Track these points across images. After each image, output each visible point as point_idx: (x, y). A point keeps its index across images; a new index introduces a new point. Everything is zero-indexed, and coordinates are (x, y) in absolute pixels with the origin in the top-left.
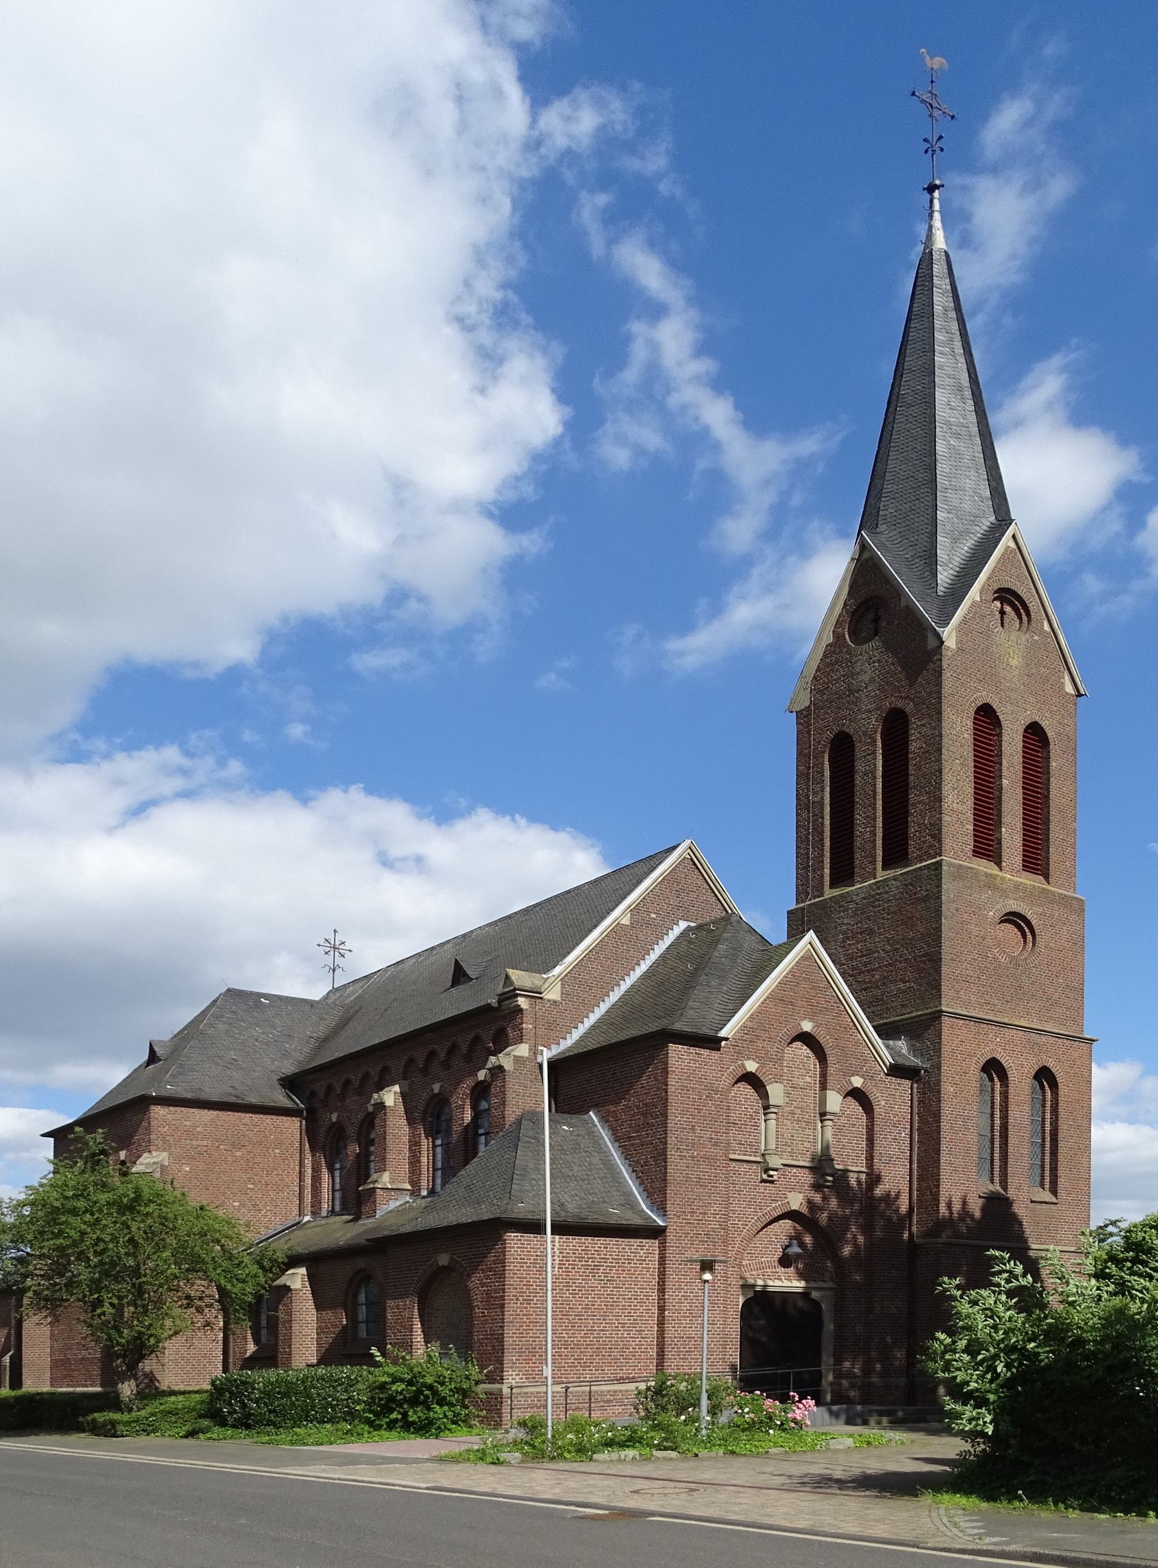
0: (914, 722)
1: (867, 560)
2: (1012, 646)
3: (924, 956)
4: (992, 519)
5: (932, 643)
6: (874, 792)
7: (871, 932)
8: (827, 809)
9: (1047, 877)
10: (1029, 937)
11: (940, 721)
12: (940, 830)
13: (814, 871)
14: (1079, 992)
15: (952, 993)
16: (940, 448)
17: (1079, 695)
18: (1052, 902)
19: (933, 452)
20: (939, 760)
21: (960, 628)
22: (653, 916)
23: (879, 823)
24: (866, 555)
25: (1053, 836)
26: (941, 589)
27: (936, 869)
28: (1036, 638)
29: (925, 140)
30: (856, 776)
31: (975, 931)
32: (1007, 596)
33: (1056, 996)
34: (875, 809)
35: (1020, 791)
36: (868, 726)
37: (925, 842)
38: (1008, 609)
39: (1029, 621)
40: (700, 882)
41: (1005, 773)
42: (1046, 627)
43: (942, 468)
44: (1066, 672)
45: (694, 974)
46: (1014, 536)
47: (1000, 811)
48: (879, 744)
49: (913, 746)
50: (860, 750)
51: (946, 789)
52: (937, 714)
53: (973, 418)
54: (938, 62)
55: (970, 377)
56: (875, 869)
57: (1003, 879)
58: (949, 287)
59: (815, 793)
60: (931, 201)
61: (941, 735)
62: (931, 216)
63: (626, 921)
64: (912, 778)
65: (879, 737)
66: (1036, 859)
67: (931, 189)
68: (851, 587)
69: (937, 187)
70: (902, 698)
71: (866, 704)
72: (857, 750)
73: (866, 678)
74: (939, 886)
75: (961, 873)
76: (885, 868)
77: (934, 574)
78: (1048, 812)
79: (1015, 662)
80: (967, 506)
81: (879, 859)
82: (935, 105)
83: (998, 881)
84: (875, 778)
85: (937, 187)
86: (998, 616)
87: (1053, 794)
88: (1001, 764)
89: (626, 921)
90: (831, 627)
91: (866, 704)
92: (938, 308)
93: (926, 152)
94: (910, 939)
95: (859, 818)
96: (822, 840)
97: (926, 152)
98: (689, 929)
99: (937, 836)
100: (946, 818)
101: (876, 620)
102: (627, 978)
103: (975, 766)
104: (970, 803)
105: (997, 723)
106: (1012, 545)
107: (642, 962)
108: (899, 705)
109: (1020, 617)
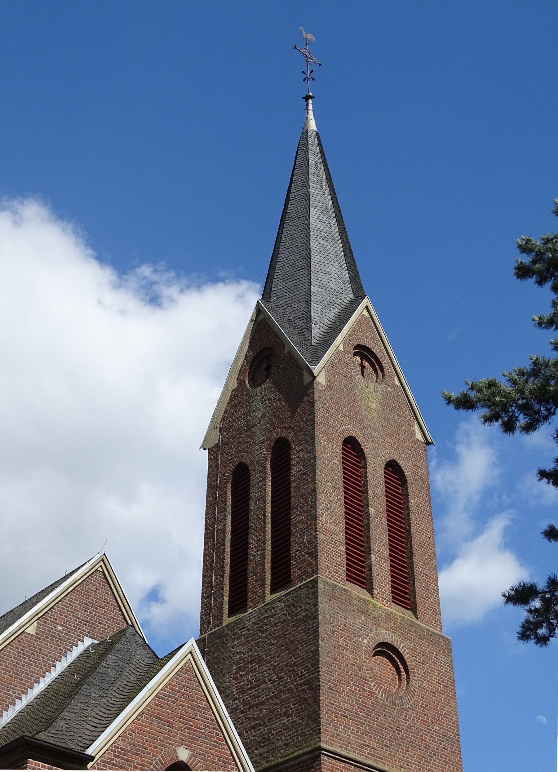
0: (295, 448)
1: (261, 321)
2: (370, 393)
3: (304, 684)
4: (352, 296)
5: (307, 379)
6: (264, 515)
7: (260, 660)
8: (228, 537)
9: (414, 611)
10: (403, 673)
11: (314, 444)
12: (316, 547)
13: (215, 599)
14: (454, 742)
15: (331, 729)
17: (428, 443)
18: (421, 637)
20: (314, 480)
21: (331, 365)
22: (60, 628)
23: (268, 546)
24: (261, 317)
25: (417, 570)
27: (313, 587)
28: (389, 389)
29: (303, 72)
30: (251, 502)
31: (351, 658)
32: (363, 352)
33: (434, 746)
34: (264, 532)
36: (261, 455)
37: (304, 561)
38: (366, 364)
39: (383, 375)
40: (109, 598)
41: (371, 502)
42: (397, 382)
43: (315, 258)
44: (415, 422)
45: (79, 684)
47: (368, 537)
49: (294, 470)
50: (255, 477)
51: (320, 508)
52: (310, 439)
53: (336, 229)
54: (309, 36)
55: (333, 203)
56: (264, 593)
57: (375, 606)
58: (319, 151)
59: (219, 521)
60: (307, 105)
61: (314, 458)
62: (307, 112)
63: (31, 630)
64: (293, 499)
65: (268, 465)
66: (404, 592)
67: (307, 98)
70: (286, 428)
71: (260, 436)
72: (252, 478)
73: (259, 414)
74: (316, 605)
75: (335, 594)
76: (273, 591)
77: (309, 330)
78: (411, 546)
79: (374, 406)
80: (333, 285)
81: (268, 582)
82: (309, 56)
83: (370, 607)
84: (265, 502)
86: (359, 368)
87: (414, 529)
88: (367, 493)
89: (31, 630)
90: (236, 376)
91: (260, 436)
92: (311, 162)
93: (304, 80)
94: (292, 666)
95: (252, 542)
96: (223, 567)
97: (304, 80)
98: (93, 646)
99: (314, 555)
100: (321, 536)
101: (268, 369)
102: (23, 696)
105: (362, 456)
106: (365, 313)
107: (41, 679)
108: (283, 434)
109: (376, 372)
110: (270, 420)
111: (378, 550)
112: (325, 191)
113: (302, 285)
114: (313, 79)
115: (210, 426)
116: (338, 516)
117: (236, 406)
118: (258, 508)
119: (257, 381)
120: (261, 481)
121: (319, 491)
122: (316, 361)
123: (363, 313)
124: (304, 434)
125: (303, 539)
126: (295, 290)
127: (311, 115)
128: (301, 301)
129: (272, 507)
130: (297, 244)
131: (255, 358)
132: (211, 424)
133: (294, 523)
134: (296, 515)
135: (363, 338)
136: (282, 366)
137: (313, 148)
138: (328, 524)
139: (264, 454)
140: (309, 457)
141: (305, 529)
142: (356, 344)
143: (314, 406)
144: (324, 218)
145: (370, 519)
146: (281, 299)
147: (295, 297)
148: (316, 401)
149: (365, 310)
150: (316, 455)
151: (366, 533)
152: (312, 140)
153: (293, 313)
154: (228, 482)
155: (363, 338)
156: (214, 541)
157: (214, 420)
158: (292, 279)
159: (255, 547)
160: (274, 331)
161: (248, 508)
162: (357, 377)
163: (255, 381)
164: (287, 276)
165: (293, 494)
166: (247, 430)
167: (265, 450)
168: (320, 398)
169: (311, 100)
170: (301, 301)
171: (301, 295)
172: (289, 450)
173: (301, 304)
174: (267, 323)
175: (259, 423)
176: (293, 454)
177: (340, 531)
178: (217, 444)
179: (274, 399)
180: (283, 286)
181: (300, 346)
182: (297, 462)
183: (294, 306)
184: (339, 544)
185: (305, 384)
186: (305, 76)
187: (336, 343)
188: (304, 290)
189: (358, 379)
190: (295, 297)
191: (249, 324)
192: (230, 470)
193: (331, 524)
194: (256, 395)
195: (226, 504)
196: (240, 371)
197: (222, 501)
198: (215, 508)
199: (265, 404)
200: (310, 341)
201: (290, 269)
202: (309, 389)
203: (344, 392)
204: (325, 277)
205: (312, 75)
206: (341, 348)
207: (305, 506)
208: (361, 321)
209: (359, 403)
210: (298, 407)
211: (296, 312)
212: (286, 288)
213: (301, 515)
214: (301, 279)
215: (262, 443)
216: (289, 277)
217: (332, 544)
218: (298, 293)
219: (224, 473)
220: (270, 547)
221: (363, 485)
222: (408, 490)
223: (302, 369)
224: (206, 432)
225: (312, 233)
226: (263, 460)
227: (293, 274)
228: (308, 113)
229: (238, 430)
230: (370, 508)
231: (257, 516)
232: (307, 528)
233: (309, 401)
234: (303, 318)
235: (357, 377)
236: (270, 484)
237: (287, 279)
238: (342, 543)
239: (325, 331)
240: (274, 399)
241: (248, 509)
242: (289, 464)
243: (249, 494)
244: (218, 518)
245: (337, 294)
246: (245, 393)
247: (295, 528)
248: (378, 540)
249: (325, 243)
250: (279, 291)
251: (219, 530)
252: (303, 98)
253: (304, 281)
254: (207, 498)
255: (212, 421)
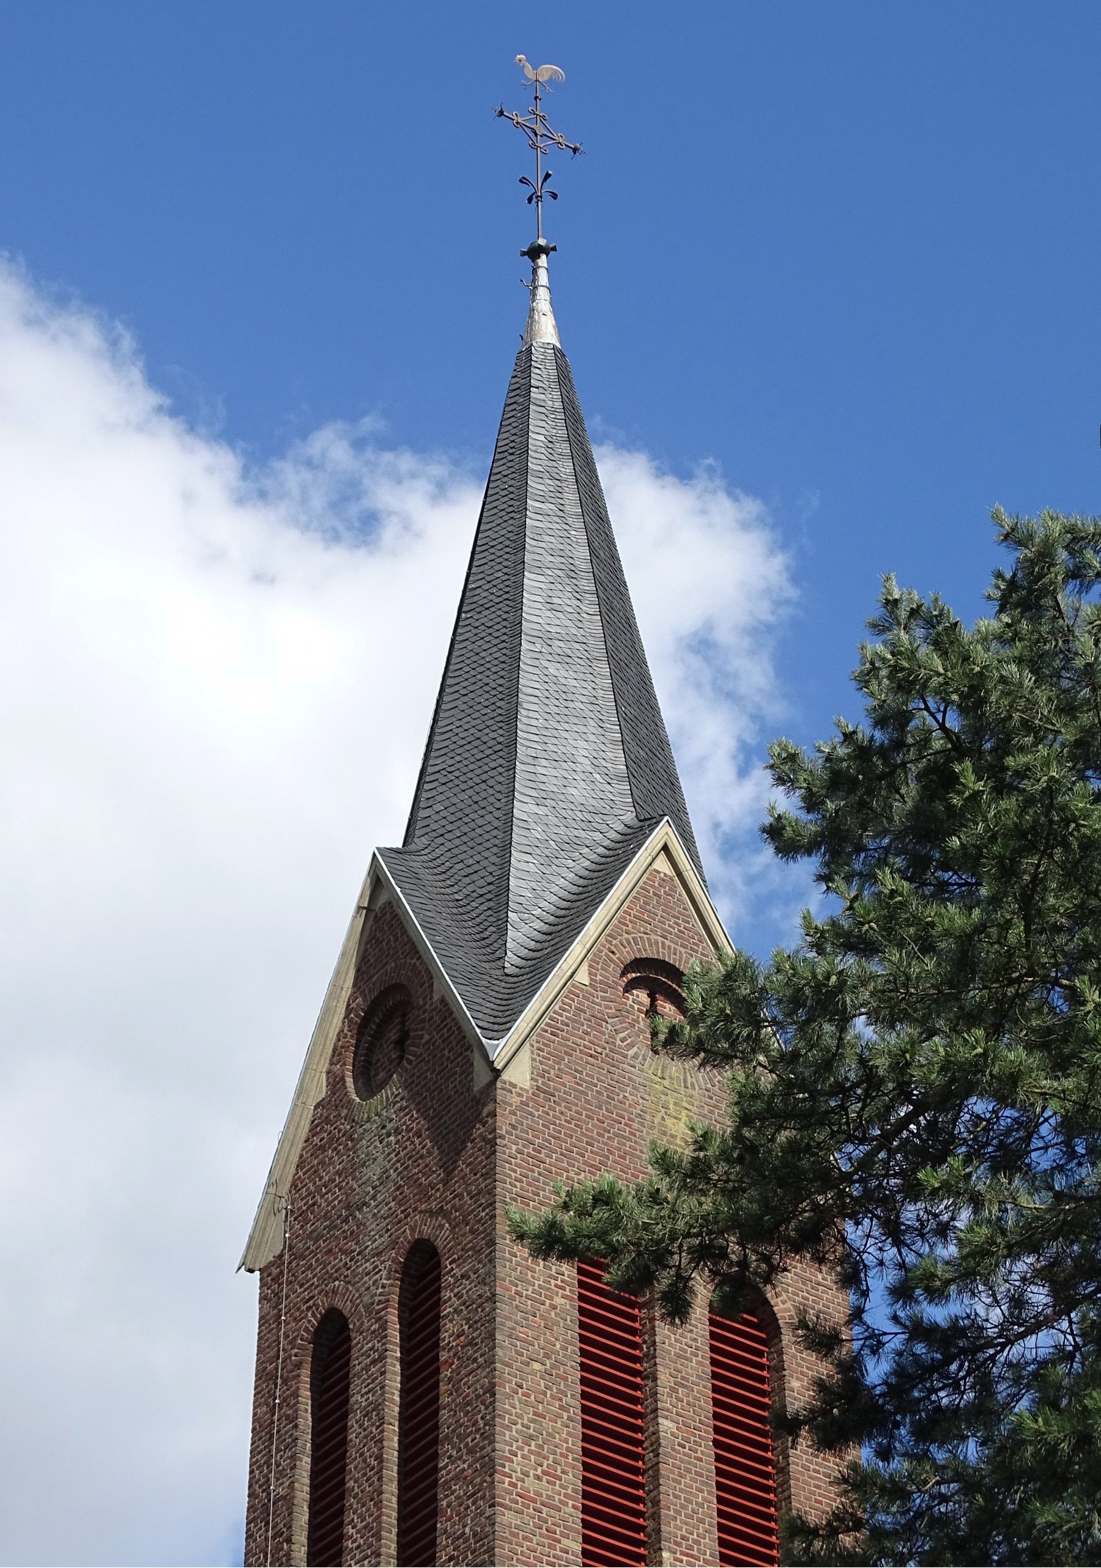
1: (383, 909)
5: (481, 1077)
6: (380, 1458)
16: (527, 681)
19: (513, 691)
21: (550, 1028)
24: (383, 899)
26: (511, 959)
34: (379, 1504)
35: (707, 1452)
36: (374, 1291)
41: (665, 1401)
46: (665, 848)
47: (656, 1503)
48: (394, 1333)
49: (449, 1329)
50: (361, 1345)
51: (507, 1439)
53: (595, 626)
55: (592, 551)
58: (558, 405)
60: (535, 271)
61: (493, 1298)
62: (534, 295)
64: (444, 1414)
65: (393, 1317)
67: (534, 252)
68: (358, 970)
69: (545, 250)
70: (432, 1213)
73: (373, 1172)
82: (541, 130)
84: (382, 1421)
85: (545, 250)
88: (655, 1379)
92: (537, 439)
93: (530, 200)
97: (530, 200)
100: (506, 1518)
103: (584, 1381)
104: (572, 1479)
106: (662, 865)
108: (427, 1231)
110: (398, 1189)
111: (683, 1538)
112: (570, 520)
113: (492, 799)
114: (554, 196)
115: (261, 1207)
116: (562, 1455)
117: (323, 1149)
118: (366, 1437)
119: (376, 1075)
120: (374, 1362)
121: (504, 1390)
122: (501, 1026)
123: (655, 866)
124: (472, 1231)
125: (464, 1527)
126: (474, 816)
127: (543, 301)
128: (488, 845)
129: (403, 1434)
130: (486, 681)
131: (370, 1012)
132: (264, 1200)
133: (446, 1482)
134: (450, 1457)
135: (653, 937)
136: (427, 1037)
137: (545, 396)
138: (530, 1481)
139: (383, 1287)
140: (480, 1296)
141: (469, 1498)
142: (629, 959)
143: (495, 1151)
144: (564, 599)
145: (661, 1450)
146: (440, 840)
147: (472, 835)
148: (502, 1137)
149: (663, 855)
150: (499, 1290)
151: (650, 1491)
152: (543, 373)
153: (467, 880)
154: (301, 1363)
155: (653, 937)
156: (267, 1531)
157: (272, 1190)
158: (470, 783)
159: (358, 1547)
160: (410, 940)
161: (346, 1437)
162: (631, 1053)
163: (369, 1080)
164: (457, 774)
165: (445, 1399)
166: (347, 1217)
167: (384, 1273)
168: (514, 1127)
169: (544, 257)
170: (488, 845)
171: (488, 828)
172: (438, 1278)
173: (486, 854)
174: (395, 916)
175: (374, 1198)
176: (446, 1288)
177: (566, 1495)
178: (281, 1256)
179: (409, 1130)
180: (447, 803)
181: (466, 980)
182: (455, 1310)
183: (471, 861)
184: (562, 1534)
185: (476, 1089)
186: (528, 191)
187: (560, 973)
188: (497, 814)
189: (636, 1056)
190: (472, 835)
191: (355, 917)
192: (306, 1330)
193: (539, 1478)
194: (368, 1120)
195: (296, 1426)
196: (334, 1052)
197: (287, 1417)
198: (272, 1436)
199: (389, 1144)
200: (499, 963)
201: (466, 755)
202: (484, 1105)
203: (587, 1102)
204: (554, 772)
205: (549, 186)
206: (583, 977)
207: (469, 1435)
208: (643, 892)
209: (635, 1126)
210: (458, 1153)
211: (475, 877)
212: (452, 809)
213: (460, 1458)
214: (491, 782)
215: (379, 1254)
216: (463, 778)
217: (541, 1535)
218: (480, 822)
219: (295, 1338)
220: (394, 1546)
221: (647, 1355)
222: (782, 1353)
223: (469, 1048)
224: (252, 1223)
225: (525, 646)
226: (380, 1302)
227: (471, 767)
228: (534, 295)
229: (326, 1217)
230: (660, 1420)
231: (365, 1461)
232: (473, 1495)
233: (484, 1139)
234: (488, 896)
235: (631, 1053)
236: (398, 1368)
237: (457, 782)
238: (571, 1529)
239: (545, 928)
240: (409, 1130)
241: (344, 1442)
242: (437, 1317)
243: (347, 1401)
244: (278, 1466)
245: (588, 817)
246: (344, 1112)
247: (447, 1496)
248: (683, 1507)
249: (563, 673)
250: (435, 817)
251: (279, 1500)
252: (523, 254)
253: (498, 787)
254: (255, 1408)
255: (266, 1193)
